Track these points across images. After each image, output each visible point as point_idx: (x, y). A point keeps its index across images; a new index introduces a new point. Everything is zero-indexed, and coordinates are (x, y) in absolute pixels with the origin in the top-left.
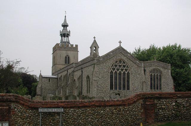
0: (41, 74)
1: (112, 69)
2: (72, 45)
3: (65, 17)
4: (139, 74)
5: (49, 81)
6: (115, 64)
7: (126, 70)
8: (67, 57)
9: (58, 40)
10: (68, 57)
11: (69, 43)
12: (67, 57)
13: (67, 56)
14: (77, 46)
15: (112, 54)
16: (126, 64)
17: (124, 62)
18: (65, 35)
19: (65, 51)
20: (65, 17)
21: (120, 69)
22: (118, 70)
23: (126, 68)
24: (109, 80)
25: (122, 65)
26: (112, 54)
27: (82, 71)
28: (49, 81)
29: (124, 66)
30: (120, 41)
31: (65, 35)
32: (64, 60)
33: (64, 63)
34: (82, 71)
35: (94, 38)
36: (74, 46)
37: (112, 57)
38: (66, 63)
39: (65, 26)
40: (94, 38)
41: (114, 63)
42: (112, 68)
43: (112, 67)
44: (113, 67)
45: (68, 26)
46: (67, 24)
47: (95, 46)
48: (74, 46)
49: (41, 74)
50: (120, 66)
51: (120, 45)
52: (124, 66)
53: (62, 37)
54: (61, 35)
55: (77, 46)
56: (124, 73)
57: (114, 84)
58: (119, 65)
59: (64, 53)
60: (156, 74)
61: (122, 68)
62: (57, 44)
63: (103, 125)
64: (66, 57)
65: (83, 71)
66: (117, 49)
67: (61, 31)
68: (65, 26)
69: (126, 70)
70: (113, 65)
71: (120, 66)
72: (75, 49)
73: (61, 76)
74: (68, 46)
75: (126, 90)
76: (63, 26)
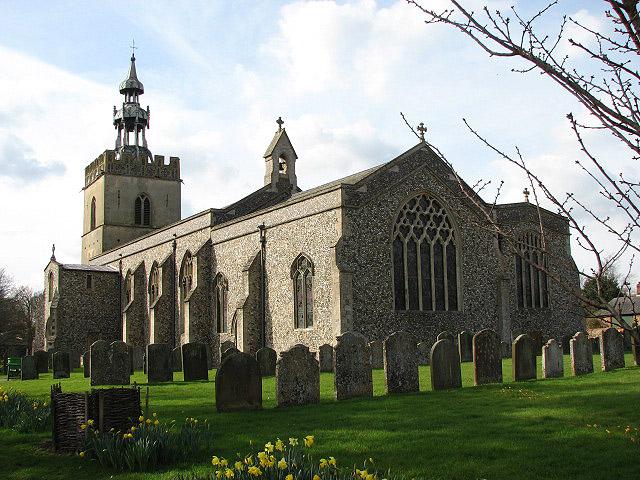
0: (53, 259)
1: (398, 232)
2: (160, 159)
3: (133, 60)
4: (485, 250)
5: (89, 286)
6: (408, 210)
7: (445, 234)
8: (143, 201)
9: (106, 138)
10: (147, 201)
11: (145, 151)
12: (143, 201)
13: (143, 197)
14: (175, 161)
15: (396, 169)
16: (444, 212)
17: (437, 206)
18: (133, 120)
19: (135, 179)
20: (133, 60)
21: (439, 229)
22: (419, 232)
23: (444, 226)
24: (392, 272)
25: (418, 214)
26: (396, 169)
27: (264, 241)
28: (89, 286)
29: (438, 220)
30: (422, 124)
31: (133, 120)
32: (131, 210)
33: (131, 220)
34: (264, 241)
35: (280, 122)
36: (167, 162)
37: (401, 183)
38: (138, 220)
39: (133, 89)
40: (280, 122)
41: (405, 208)
42: (399, 225)
43: (398, 221)
44: (402, 223)
45: (142, 92)
46: (139, 84)
47: (283, 152)
48: (167, 162)
49: (53, 259)
50: (426, 218)
51: (423, 139)
52: (438, 220)
53: (120, 131)
54: (117, 122)
55: (175, 161)
56: (438, 244)
57: (407, 287)
58: (422, 215)
59: (131, 185)
60: (531, 252)
61: (404, 222)
62: (110, 154)
63: (183, 448)
64: (138, 201)
65: (270, 241)
66: (413, 155)
67: (119, 107)
68: (133, 89)
69: (445, 234)
70: (401, 214)
71: (426, 218)
72: (169, 172)
73: (142, 265)
74: (144, 161)
75: (407, 308)
76: (122, 92)
